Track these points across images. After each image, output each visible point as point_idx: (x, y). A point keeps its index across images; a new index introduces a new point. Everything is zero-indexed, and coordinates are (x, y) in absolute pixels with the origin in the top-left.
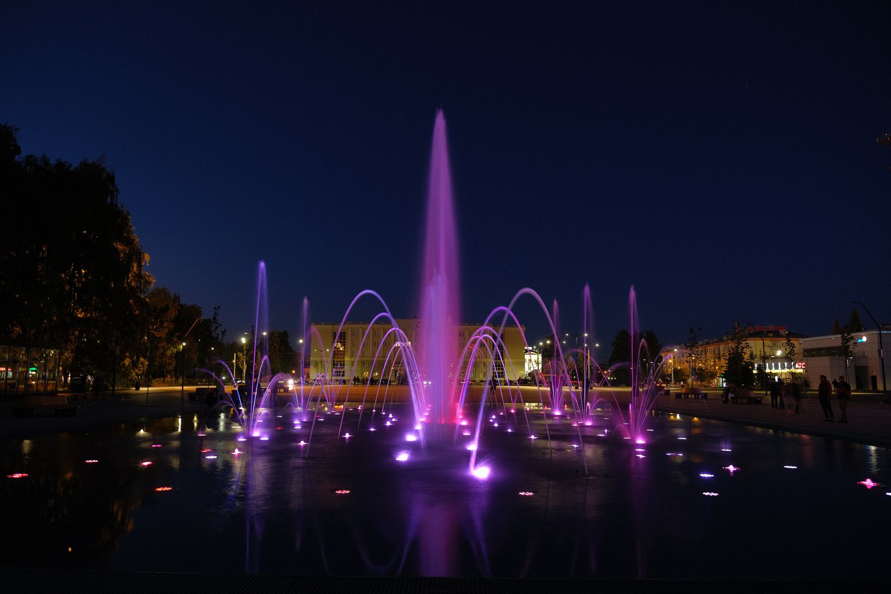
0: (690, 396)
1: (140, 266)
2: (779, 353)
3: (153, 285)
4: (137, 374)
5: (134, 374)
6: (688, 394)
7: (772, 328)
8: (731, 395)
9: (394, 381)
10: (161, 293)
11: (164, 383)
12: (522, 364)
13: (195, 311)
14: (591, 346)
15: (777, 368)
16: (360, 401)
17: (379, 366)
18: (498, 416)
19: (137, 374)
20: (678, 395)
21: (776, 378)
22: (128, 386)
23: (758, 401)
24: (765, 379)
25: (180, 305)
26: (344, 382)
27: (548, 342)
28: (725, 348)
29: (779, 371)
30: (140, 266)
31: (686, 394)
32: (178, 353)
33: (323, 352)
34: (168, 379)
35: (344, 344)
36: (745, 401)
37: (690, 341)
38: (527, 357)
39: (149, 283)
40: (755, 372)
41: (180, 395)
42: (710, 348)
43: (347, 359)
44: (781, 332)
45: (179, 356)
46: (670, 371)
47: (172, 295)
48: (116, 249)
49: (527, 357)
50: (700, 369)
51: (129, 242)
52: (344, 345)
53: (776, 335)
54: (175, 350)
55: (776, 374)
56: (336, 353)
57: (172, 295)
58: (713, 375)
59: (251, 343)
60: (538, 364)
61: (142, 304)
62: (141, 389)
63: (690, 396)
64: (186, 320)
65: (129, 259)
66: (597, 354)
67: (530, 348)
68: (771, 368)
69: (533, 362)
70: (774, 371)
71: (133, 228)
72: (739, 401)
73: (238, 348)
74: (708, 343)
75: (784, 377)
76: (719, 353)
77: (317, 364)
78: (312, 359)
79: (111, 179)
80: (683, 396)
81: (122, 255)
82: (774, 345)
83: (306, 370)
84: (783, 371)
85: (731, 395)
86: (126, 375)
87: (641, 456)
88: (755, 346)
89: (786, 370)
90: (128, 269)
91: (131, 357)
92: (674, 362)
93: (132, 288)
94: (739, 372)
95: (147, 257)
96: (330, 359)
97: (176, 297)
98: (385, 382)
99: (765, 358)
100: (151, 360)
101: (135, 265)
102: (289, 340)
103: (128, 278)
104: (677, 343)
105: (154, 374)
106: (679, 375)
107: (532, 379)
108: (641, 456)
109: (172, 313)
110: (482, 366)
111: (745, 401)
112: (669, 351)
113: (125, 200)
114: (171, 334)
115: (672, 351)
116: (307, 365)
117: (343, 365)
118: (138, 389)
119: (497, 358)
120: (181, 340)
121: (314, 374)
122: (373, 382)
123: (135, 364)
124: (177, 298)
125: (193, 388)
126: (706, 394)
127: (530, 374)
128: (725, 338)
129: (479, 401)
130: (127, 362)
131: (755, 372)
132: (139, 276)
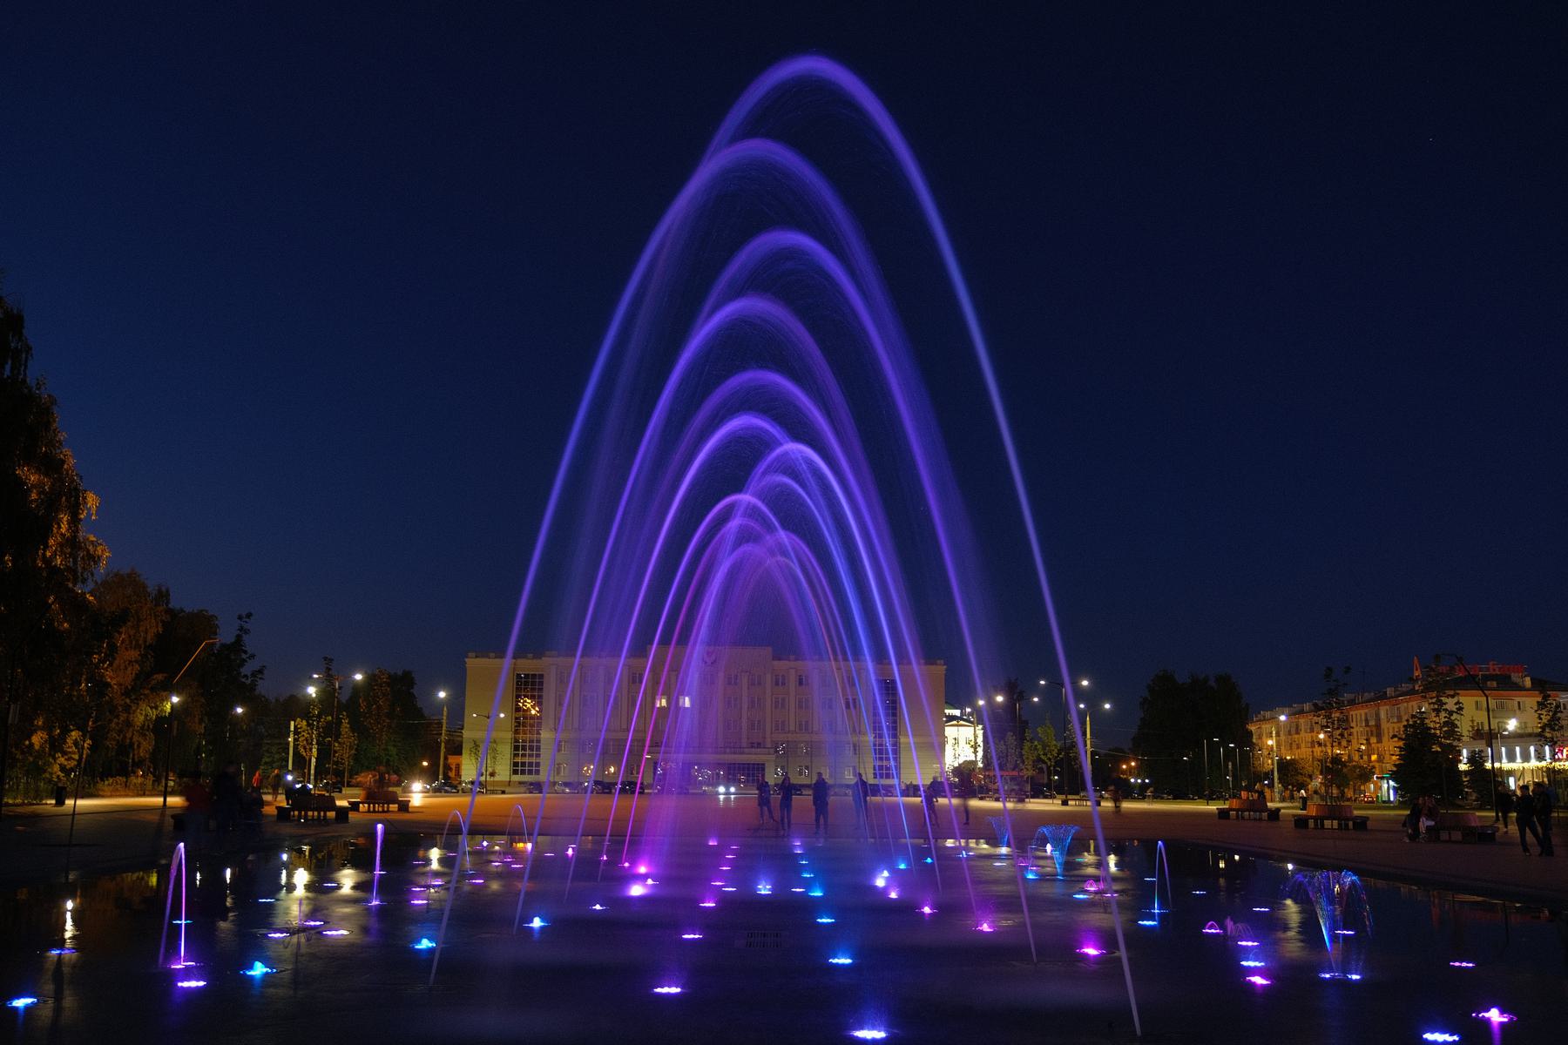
0: (1327, 823)
1: (75, 521)
2: (1512, 725)
3: (102, 568)
4: (63, 769)
5: (56, 768)
6: (1323, 819)
7: (1494, 668)
8: (1425, 823)
9: (651, 786)
10: (125, 582)
11: (128, 790)
12: (939, 746)
13: (203, 624)
14: (1088, 708)
15: (1511, 758)
16: (572, 834)
17: (610, 751)
18: (895, 872)
19: (63, 769)
20: (1301, 822)
21: (1512, 781)
22: (39, 796)
23: (1484, 836)
24: (1489, 784)
25: (170, 611)
26: (537, 787)
27: (1000, 699)
28: (1394, 717)
29: (1518, 765)
30: (75, 521)
31: (1319, 819)
32: (161, 719)
33: (487, 721)
34: (138, 778)
35: (539, 702)
36: (1457, 836)
37: (1326, 695)
38: (950, 732)
39: (95, 559)
40: (1463, 767)
41: (155, 818)
42: (1358, 715)
43: (546, 735)
44: (1515, 677)
45: (161, 726)
46: (1269, 764)
47: (152, 588)
48: (20, 482)
49: (950, 732)
50: (1336, 760)
51: (51, 465)
52: (539, 704)
53: (1506, 684)
54: (153, 714)
55: (1510, 773)
56: (521, 721)
57: (152, 588)
58: (1366, 776)
59: (328, 694)
60: (975, 747)
61: (76, 605)
62: (69, 802)
63: (1327, 823)
64: (180, 645)
65: (51, 504)
66: (1102, 725)
67: (957, 712)
68: (1496, 757)
69: (963, 744)
70: (1506, 765)
71: (62, 436)
72: (1444, 836)
73: (297, 707)
74: (1352, 703)
75: (1528, 778)
76: (1378, 726)
77: (476, 746)
78: (466, 734)
79: (15, 322)
80: (1311, 823)
81: (34, 496)
82: (1501, 707)
83: (452, 760)
84: (1526, 765)
85: (1425, 823)
86: (37, 770)
87: (1258, 980)
88: (1470, 709)
89: (1534, 763)
90: (43, 529)
91: (48, 728)
92: (1278, 745)
93: (54, 570)
94: (1424, 764)
95: (92, 500)
96: (509, 735)
97: (160, 591)
98: (629, 787)
99: (1490, 736)
100: (98, 737)
101: (65, 518)
102: (415, 691)
103: (46, 547)
104: (1274, 704)
105: (104, 768)
106: (1290, 773)
107: (966, 781)
108: (1258, 980)
109: (151, 629)
110: (849, 752)
111: (1457, 836)
112: (1265, 720)
113: (44, 371)
114: (142, 679)
115: (1274, 718)
116: (457, 749)
117: (535, 747)
118: (60, 803)
119: (880, 752)
120: (170, 689)
121: (469, 770)
122: (605, 787)
123: (56, 745)
124: (163, 596)
125: (1213, 807)
126: (1365, 819)
127: (957, 771)
128: (1389, 691)
129: (894, 682)
130: (37, 739)
131: (1463, 767)
132: (72, 544)
